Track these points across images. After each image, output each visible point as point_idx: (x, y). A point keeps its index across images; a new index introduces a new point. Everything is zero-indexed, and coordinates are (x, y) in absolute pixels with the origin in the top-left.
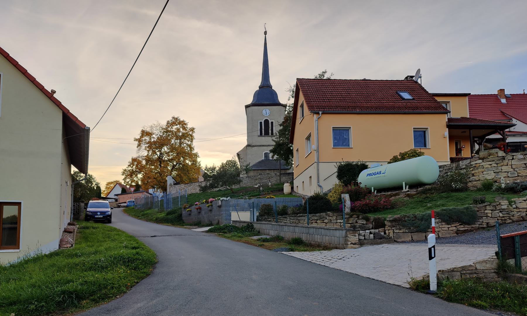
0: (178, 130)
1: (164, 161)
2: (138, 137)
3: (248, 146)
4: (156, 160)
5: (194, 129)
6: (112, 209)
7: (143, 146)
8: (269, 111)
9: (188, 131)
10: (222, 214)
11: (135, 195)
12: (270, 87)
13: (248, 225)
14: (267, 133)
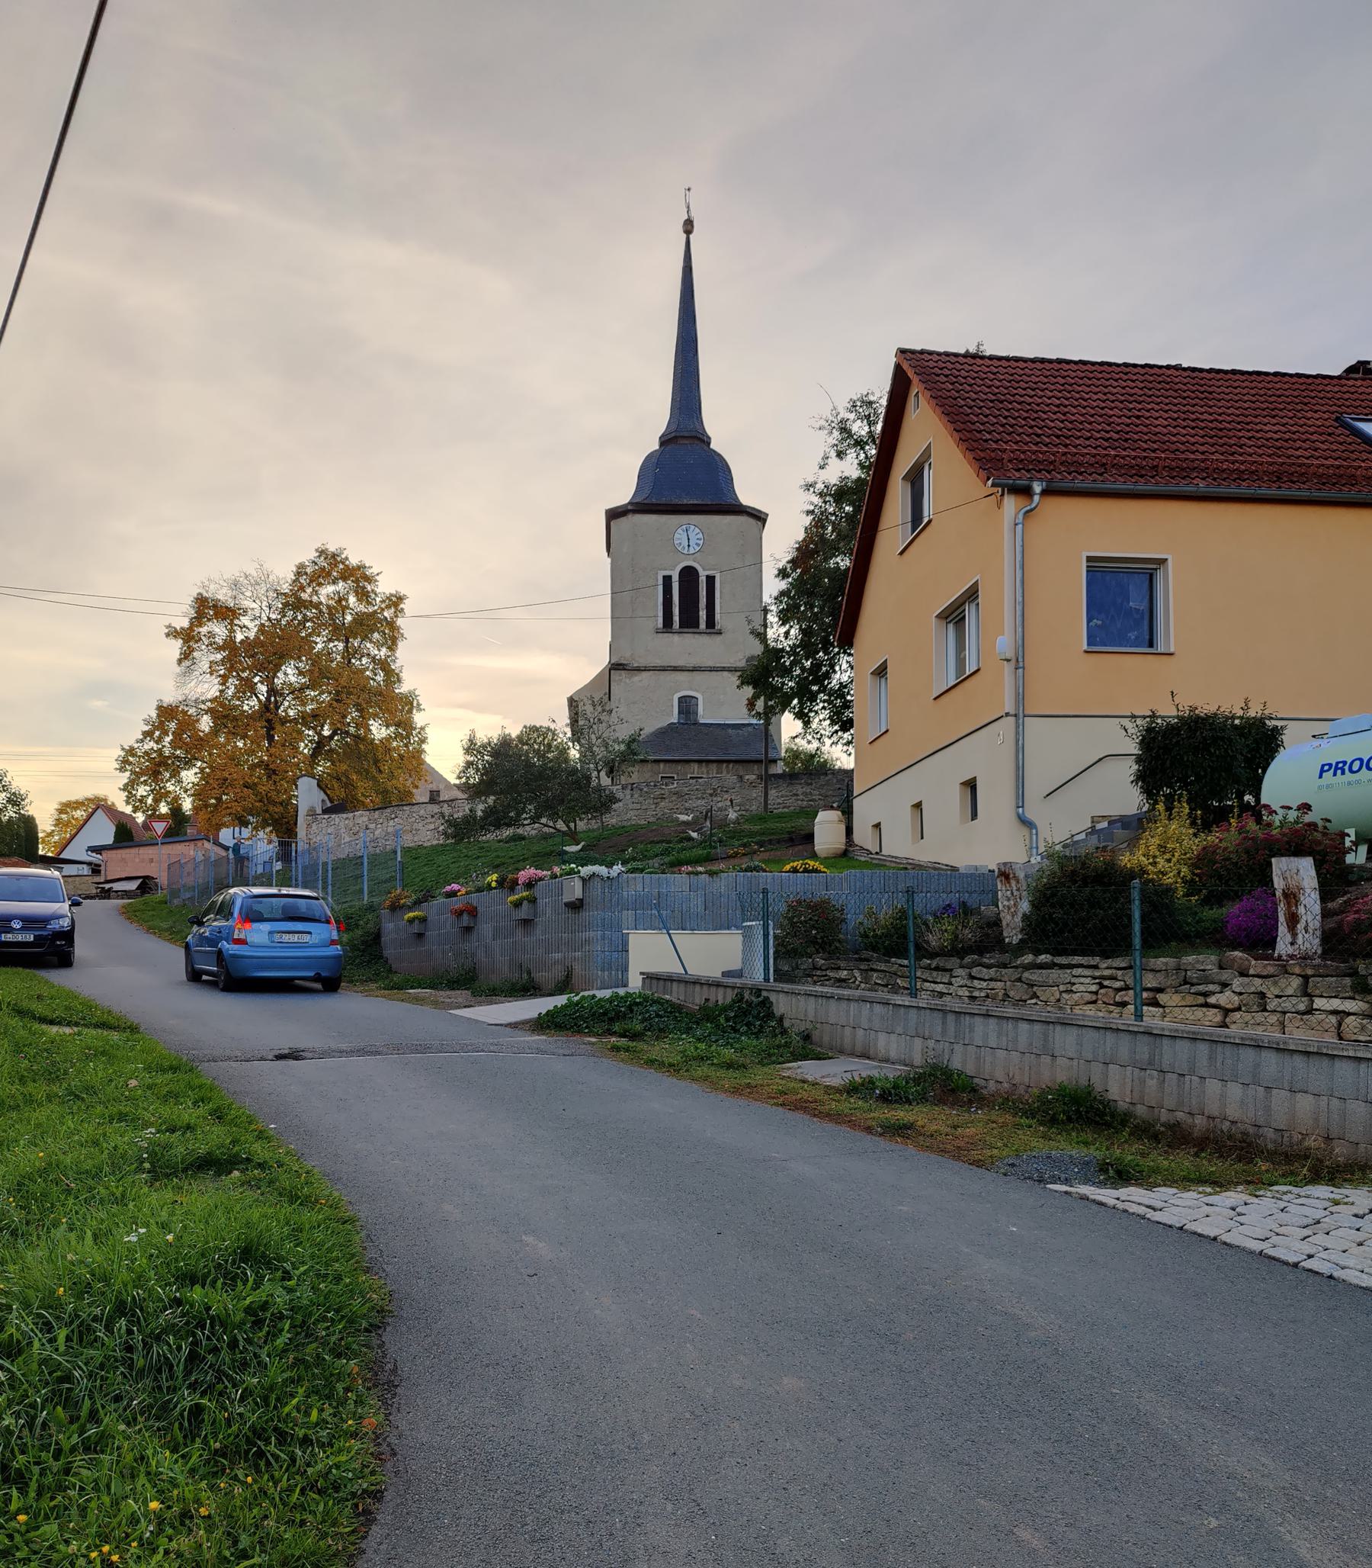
0: (340, 601)
1: (284, 721)
2: (185, 623)
3: (615, 667)
4: (251, 717)
5: (401, 599)
6: (75, 904)
7: (205, 657)
8: (700, 536)
9: (380, 607)
10: (588, 941)
11: (167, 850)
12: (704, 440)
13: (740, 998)
14: (689, 622)
